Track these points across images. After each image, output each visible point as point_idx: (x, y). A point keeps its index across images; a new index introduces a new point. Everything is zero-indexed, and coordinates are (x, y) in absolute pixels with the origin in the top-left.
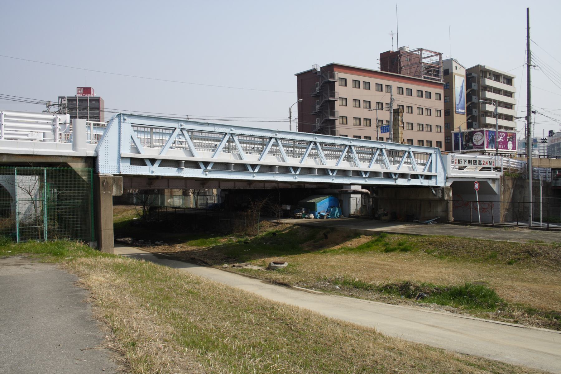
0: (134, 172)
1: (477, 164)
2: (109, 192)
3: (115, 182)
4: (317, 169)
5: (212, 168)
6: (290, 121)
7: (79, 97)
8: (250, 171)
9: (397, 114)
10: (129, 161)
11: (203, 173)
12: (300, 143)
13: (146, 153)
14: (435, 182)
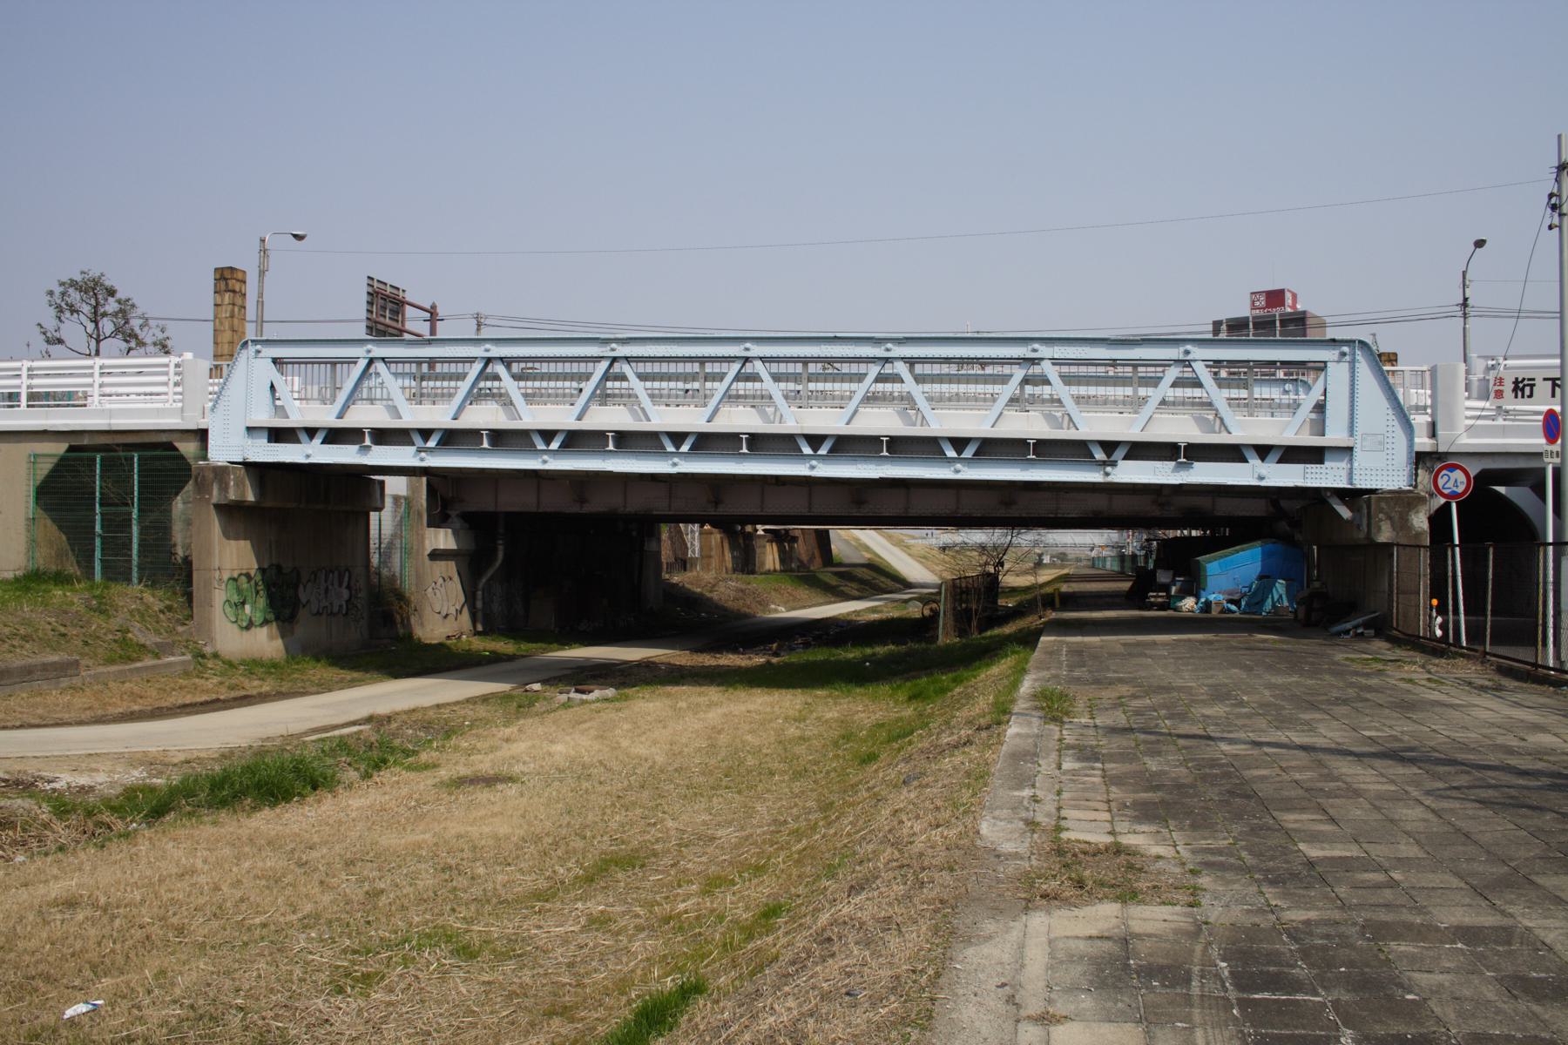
0: (1318, 481)
5: (831, 451)
6: (1465, 316)
7: (1254, 318)
8: (539, 448)
10: (266, 434)
11: (414, 456)
12: (1234, 373)
13: (297, 417)
14: (1344, 474)
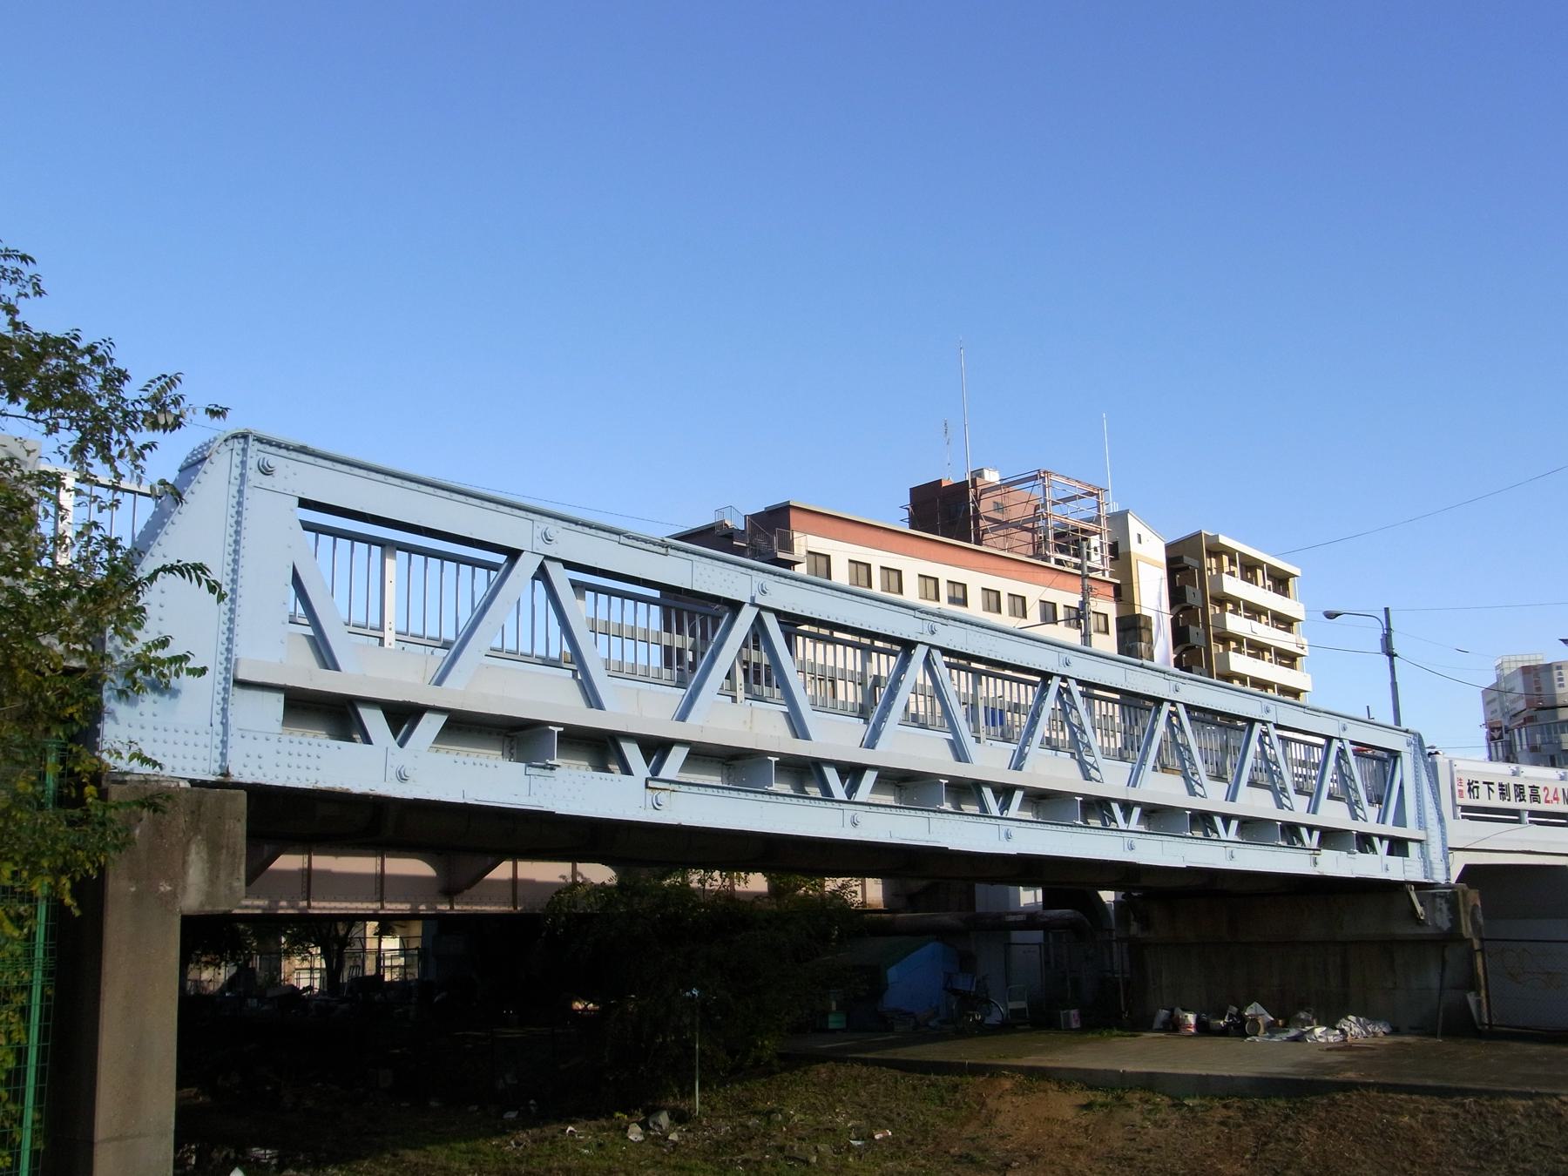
1: (1527, 798)
2: (165, 888)
3: (204, 827)
4: (1079, 799)
9: (1131, 633)
